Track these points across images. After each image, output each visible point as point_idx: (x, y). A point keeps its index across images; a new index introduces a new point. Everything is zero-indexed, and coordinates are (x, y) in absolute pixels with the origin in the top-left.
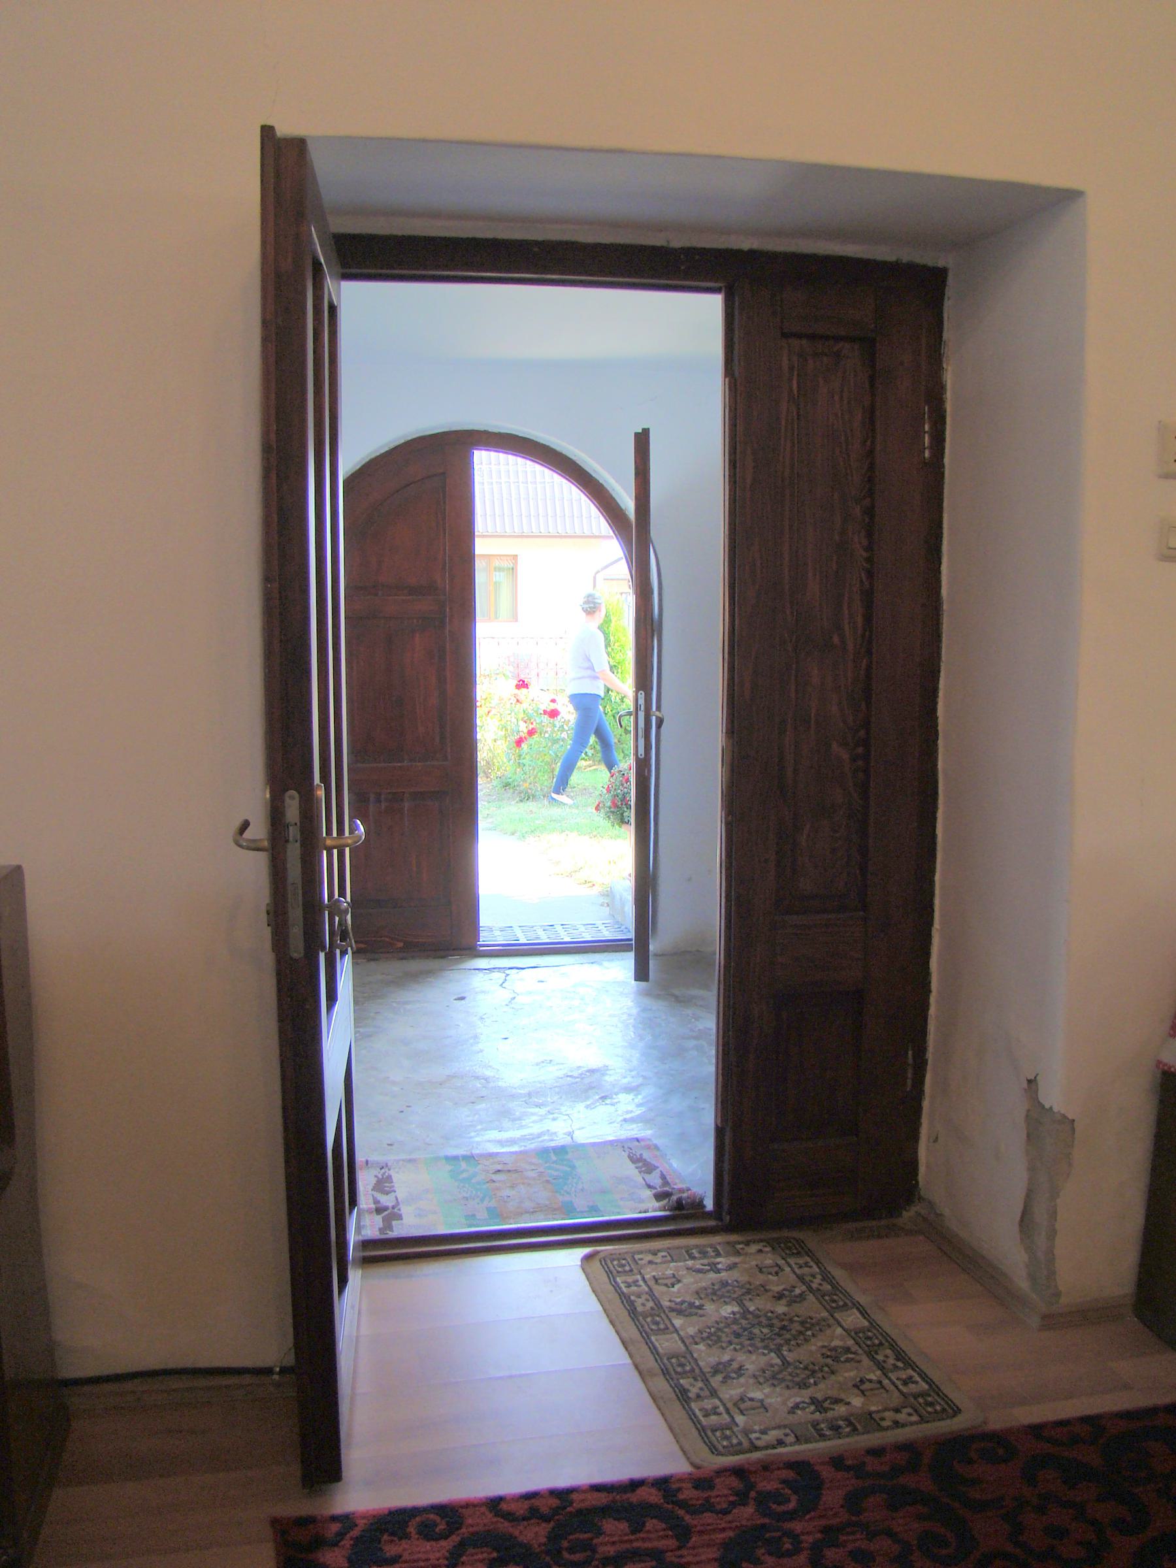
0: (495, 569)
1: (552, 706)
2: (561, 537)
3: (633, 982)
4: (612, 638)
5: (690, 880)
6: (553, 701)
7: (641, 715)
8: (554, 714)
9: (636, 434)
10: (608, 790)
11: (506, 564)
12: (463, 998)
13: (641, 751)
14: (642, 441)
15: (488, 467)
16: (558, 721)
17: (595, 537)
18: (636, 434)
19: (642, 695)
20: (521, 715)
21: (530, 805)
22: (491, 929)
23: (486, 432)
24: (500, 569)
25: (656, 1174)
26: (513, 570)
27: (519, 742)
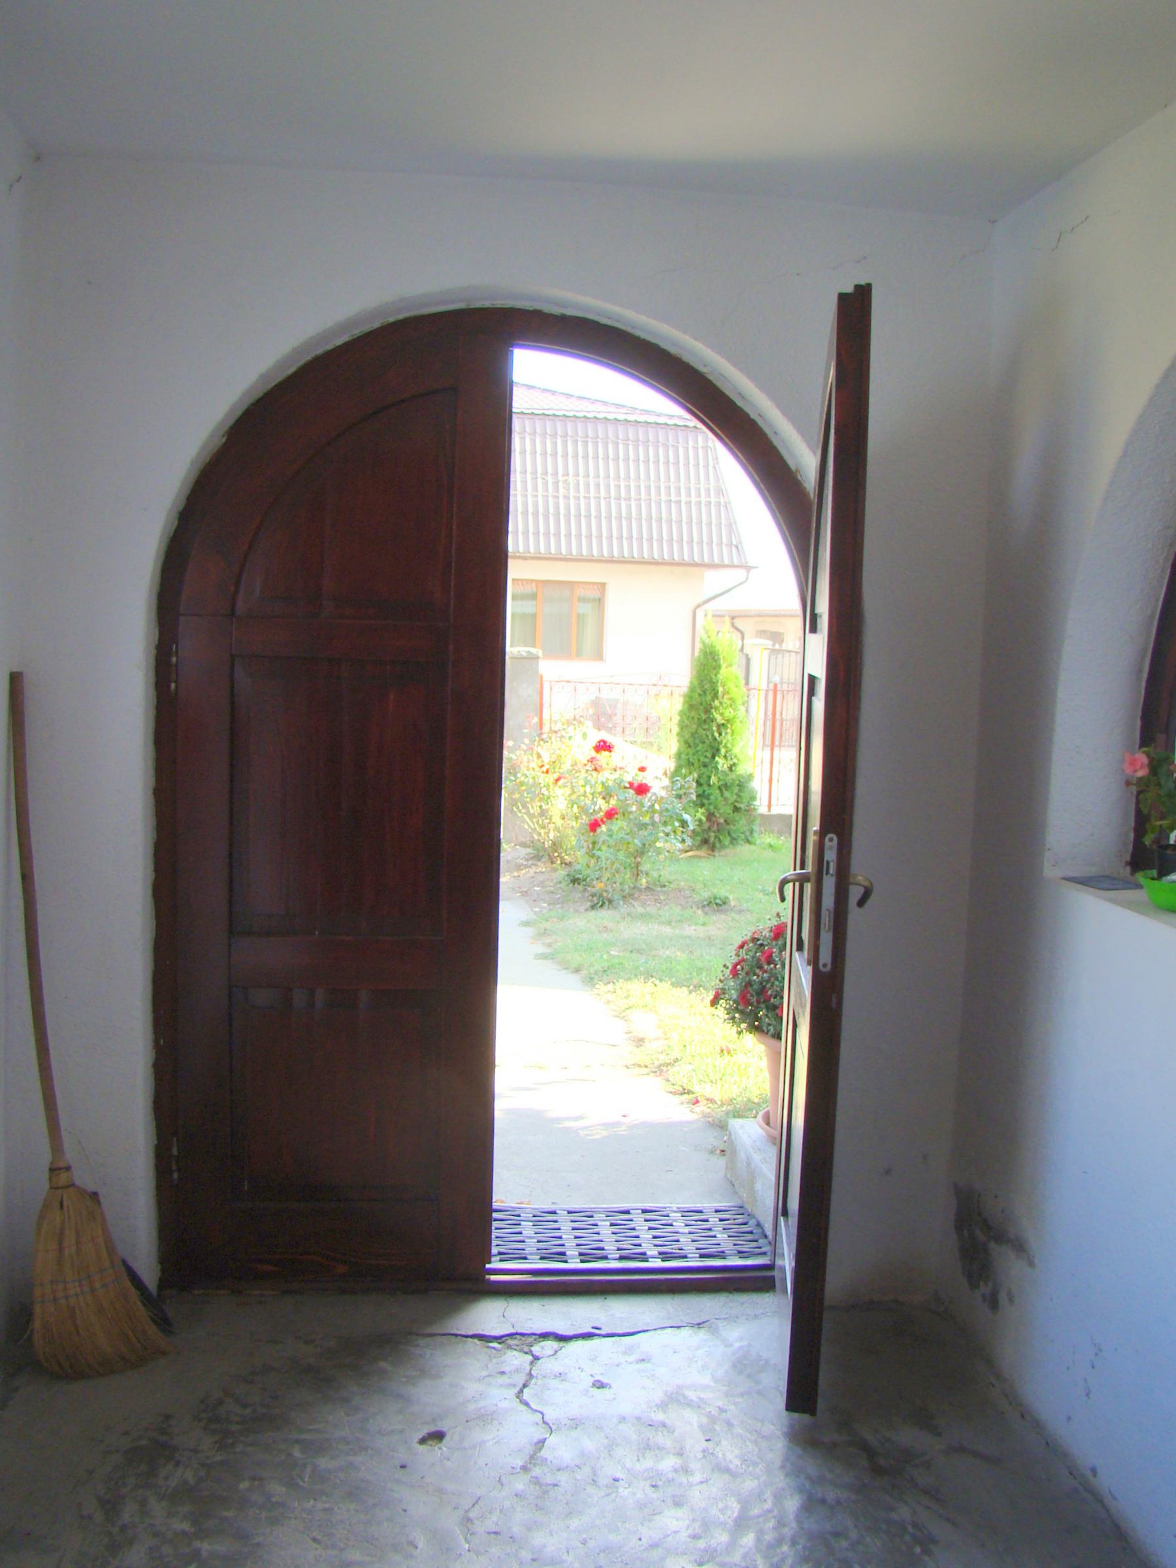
0: (579, 600)
1: (641, 778)
2: (657, 563)
3: (785, 1413)
4: (720, 689)
5: (888, 1172)
6: (642, 769)
7: (829, 884)
8: (642, 789)
9: (842, 297)
10: (734, 972)
11: (593, 593)
12: (439, 1436)
13: (826, 956)
14: (854, 311)
15: (538, 377)
16: (646, 800)
17: (697, 565)
18: (842, 297)
19: (832, 841)
20: (599, 788)
21: (604, 916)
22: (515, 1216)
23: (537, 314)
24: (584, 600)
25: (703, 1102)
26: (600, 602)
27: (594, 826)
